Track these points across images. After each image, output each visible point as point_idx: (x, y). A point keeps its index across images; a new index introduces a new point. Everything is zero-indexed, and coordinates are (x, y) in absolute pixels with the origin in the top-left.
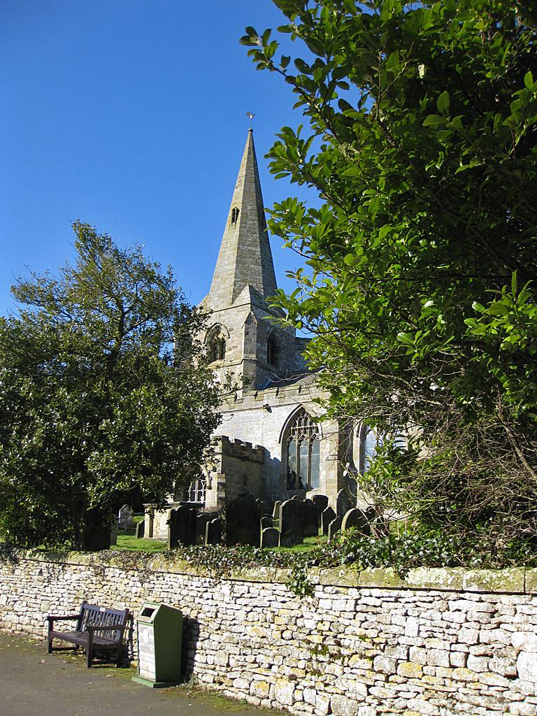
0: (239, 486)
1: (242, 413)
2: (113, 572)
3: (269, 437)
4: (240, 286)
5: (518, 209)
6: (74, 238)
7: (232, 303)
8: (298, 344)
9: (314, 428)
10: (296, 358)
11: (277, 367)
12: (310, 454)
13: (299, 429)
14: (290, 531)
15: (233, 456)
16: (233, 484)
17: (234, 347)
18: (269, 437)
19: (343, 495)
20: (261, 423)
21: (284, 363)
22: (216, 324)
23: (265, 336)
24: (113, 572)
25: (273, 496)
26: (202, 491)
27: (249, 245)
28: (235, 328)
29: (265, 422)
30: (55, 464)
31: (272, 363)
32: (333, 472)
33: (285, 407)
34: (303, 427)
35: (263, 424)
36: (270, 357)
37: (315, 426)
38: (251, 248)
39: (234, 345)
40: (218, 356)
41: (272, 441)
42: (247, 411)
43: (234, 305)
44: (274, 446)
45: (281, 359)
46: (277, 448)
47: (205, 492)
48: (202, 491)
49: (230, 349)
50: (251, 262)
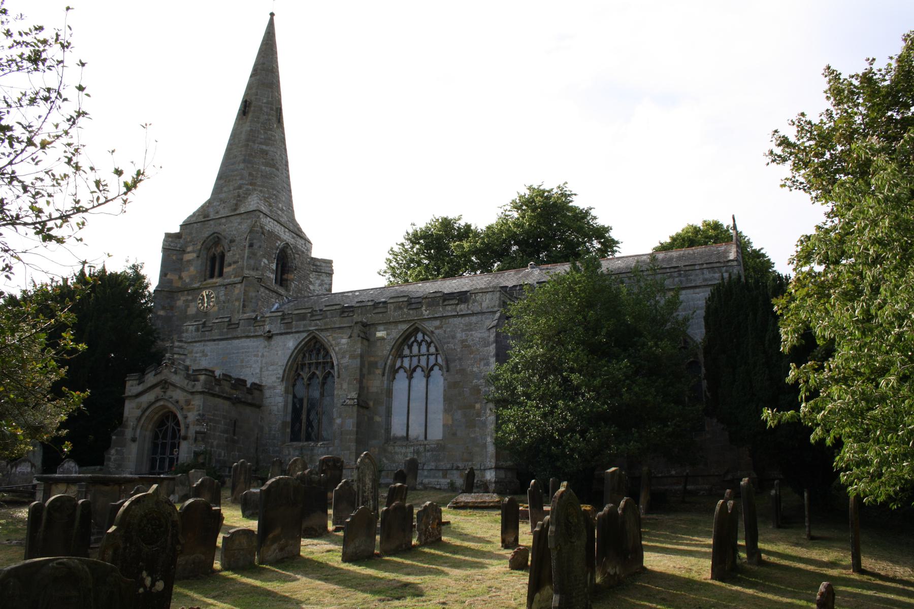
0: (226, 435)
1: (237, 341)
2: (49, 282)
3: (271, 373)
5: (732, 239)
6: (824, 84)
7: (235, 210)
9: (328, 363)
10: (311, 282)
15: (219, 396)
16: (218, 434)
17: (235, 262)
18: (271, 373)
20: (260, 354)
21: (296, 286)
22: (214, 233)
23: (274, 251)
24: (49, 282)
25: (271, 448)
27: (261, 143)
28: (237, 239)
29: (265, 354)
31: (281, 285)
34: (315, 361)
35: (263, 356)
37: (329, 360)
38: (264, 147)
39: (235, 259)
40: (303, 434)
41: (274, 378)
42: (243, 340)
45: (293, 280)
46: (279, 387)
49: (230, 265)
50: (263, 163)
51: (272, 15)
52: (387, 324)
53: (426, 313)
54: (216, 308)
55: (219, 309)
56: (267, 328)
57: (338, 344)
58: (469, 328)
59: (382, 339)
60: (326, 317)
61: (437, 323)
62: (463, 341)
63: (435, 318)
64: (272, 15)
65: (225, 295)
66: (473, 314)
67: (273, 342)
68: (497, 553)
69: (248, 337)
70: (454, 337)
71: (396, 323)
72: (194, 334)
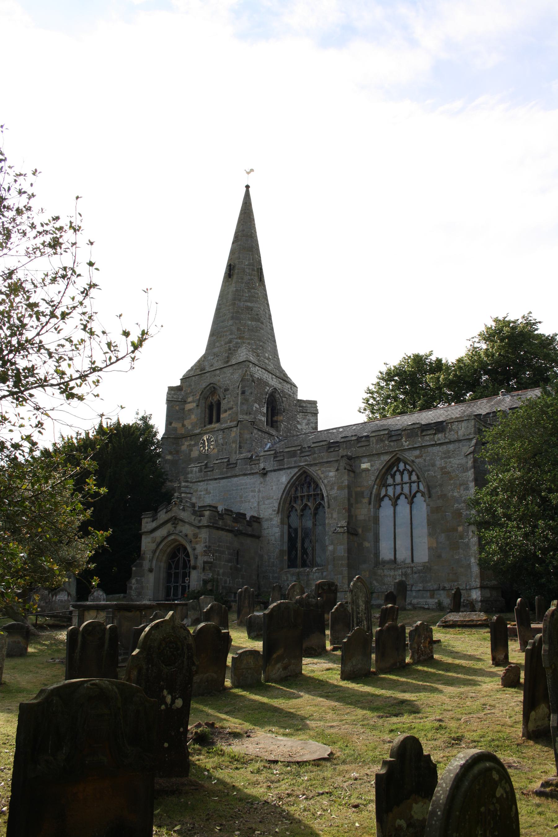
0: (230, 564)
1: (235, 479)
4: (237, 343)
7: (228, 362)
8: (300, 406)
9: (318, 494)
10: (298, 422)
11: (278, 430)
12: (376, 454)
13: (302, 497)
14: (280, 652)
19: (359, 584)
20: (257, 490)
23: (264, 396)
26: (187, 571)
27: (246, 301)
28: (231, 388)
29: (261, 489)
30: (512, 492)
31: (272, 426)
32: (342, 547)
33: (284, 471)
34: (306, 494)
35: (259, 491)
36: (270, 420)
38: (249, 304)
39: (230, 406)
41: (270, 511)
43: (230, 364)
44: (272, 516)
45: (282, 421)
47: (189, 572)
48: (187, 571)
50: (248, 318)
51: (248, 187)
52: (371, 456)
53: (406, 444)
54: (216, 450)
55: (218, 451)
56: (262, 466)
57: (326, 477)
58: (447, 455)
59: (367, 470)
60: (315, 453)
61: (417, 452)
62: (442, 468)
63: (415, 448)
64: (248, 187)
65: (223, 438)
66: (450, 442)
67: (268, 478)
68: (488, 670)
69: (245, 475)
70: (433, 465)
71: (379, 454)
72: (198, 474)
